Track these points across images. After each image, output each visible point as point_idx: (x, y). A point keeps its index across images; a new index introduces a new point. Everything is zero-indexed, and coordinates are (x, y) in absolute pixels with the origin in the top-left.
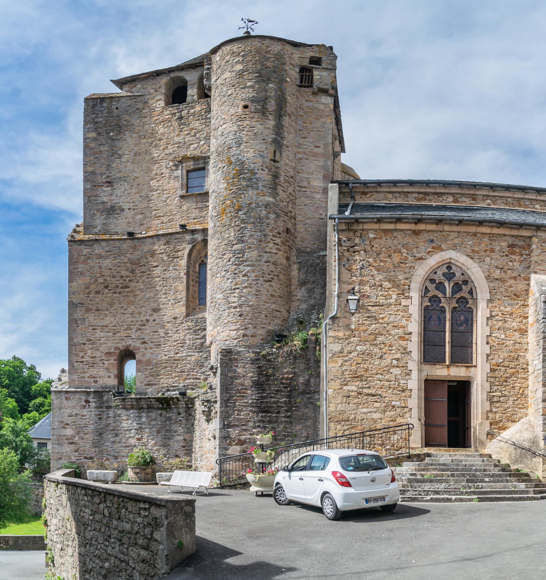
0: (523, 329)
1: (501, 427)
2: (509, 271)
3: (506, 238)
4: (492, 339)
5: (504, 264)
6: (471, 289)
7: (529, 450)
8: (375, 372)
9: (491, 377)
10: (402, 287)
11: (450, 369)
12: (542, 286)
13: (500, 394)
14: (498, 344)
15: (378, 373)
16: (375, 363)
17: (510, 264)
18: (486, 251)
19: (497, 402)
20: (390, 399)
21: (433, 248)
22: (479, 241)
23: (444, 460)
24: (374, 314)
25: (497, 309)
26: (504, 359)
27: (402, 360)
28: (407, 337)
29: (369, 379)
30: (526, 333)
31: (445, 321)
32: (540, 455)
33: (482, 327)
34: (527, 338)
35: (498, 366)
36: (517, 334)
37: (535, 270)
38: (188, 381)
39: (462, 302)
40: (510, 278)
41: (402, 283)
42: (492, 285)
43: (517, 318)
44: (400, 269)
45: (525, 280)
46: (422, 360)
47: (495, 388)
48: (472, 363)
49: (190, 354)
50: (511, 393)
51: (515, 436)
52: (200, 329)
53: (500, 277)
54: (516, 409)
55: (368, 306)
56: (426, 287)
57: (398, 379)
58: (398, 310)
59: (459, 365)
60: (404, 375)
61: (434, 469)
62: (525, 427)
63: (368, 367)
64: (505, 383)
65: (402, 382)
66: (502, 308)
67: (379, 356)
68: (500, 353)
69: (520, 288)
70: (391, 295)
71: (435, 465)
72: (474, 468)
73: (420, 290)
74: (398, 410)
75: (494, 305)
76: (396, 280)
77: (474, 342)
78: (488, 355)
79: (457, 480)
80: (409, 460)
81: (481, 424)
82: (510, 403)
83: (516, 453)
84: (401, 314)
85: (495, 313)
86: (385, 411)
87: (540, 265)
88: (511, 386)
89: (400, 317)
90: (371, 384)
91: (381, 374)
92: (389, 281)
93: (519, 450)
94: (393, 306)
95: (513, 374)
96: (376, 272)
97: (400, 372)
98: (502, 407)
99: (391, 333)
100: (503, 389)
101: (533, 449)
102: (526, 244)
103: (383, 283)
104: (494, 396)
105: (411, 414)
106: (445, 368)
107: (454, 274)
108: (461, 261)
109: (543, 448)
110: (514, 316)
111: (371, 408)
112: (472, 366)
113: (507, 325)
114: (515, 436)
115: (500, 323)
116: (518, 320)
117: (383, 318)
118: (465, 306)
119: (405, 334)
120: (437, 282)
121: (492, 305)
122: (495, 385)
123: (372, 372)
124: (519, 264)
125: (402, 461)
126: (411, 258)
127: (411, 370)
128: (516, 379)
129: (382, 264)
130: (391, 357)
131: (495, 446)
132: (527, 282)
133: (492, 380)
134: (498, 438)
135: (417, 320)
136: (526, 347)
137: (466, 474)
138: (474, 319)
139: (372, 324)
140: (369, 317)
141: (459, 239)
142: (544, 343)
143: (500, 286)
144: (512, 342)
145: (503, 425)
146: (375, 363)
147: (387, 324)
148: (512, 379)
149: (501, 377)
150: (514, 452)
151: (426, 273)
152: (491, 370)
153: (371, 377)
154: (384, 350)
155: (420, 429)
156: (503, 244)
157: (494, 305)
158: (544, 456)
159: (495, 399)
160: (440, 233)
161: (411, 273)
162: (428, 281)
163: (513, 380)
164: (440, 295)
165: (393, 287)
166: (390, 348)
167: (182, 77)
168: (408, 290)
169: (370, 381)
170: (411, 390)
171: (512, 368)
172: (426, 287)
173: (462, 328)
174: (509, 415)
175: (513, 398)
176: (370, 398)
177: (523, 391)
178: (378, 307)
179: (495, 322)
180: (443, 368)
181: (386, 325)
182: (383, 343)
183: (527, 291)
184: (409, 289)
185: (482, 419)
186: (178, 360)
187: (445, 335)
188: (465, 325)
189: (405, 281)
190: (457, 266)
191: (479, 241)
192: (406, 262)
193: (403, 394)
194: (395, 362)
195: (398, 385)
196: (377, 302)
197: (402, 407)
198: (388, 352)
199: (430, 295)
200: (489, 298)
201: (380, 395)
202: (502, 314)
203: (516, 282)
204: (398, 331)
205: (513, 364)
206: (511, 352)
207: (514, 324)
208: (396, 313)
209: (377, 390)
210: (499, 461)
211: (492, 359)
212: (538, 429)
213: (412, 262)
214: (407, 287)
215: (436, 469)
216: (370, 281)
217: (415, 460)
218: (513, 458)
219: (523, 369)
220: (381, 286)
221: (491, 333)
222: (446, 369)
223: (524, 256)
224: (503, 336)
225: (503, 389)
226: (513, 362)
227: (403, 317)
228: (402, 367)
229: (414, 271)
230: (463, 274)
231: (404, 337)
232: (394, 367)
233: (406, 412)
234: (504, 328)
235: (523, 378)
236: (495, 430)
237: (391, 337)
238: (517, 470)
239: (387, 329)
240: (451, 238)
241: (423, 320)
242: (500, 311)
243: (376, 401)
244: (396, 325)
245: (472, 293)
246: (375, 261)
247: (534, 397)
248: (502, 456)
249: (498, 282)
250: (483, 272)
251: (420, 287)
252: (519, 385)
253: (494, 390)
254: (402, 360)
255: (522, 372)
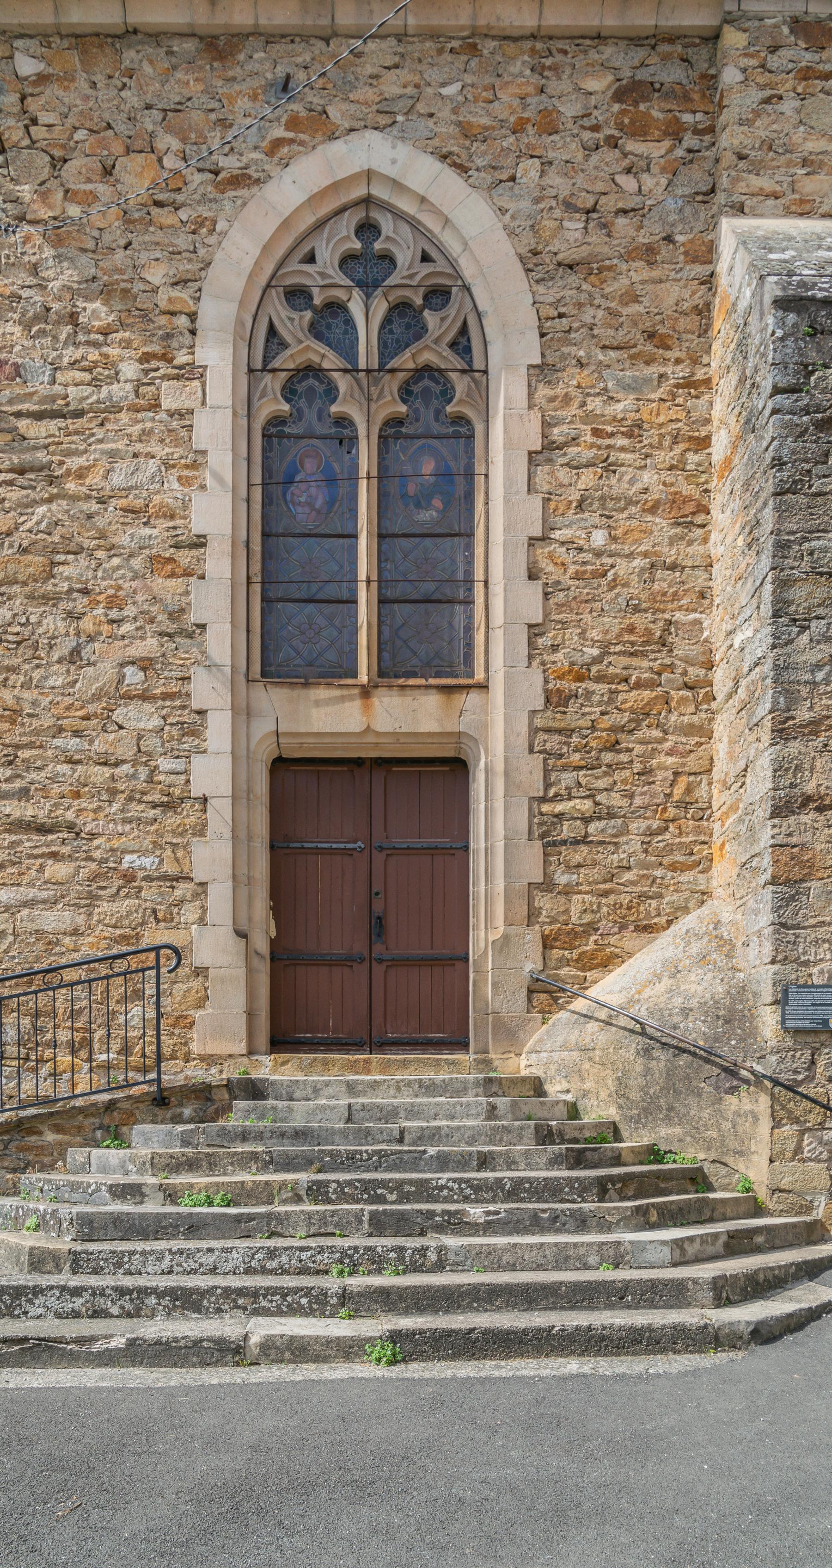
0: (687, 500)
1: (593, 956)
2: (621, 221)
3: (608, 51)
4: (550, 556)
5: (600, 187)
6: (464, 330)
7: (708, 1057)
8: (47, 721)
9: (548, 730)
10: (163, 320)
11: (375, 700)
12: (771, 250)
13: (586, 806)
14: (578, 576)
15: (61, 730)
16: (51, 682)
17: (628, 183)
18: (518, 129)
19: (576, 842)
20: (115, 843)
21: (293, 123)
22: (488, 80)
23: (311, 1114)
24: (42, 456)
25: (573, 409)
26: (605, 647)
27: (165, 664)
28: (185, 557)
29: (24, 754)
30: (700, 519)
31: (354, 479)
32: (759, 1078)
33: (507, 500)
34: (705, 540)
35: (580, 678)
36: (660, 523)
37: (737, 198)
39: (426, 393)
40: (629, 256)
41: (163, 305)
42: (548, 294)
43: (660, 447)
44: (154, 235)
45: (695, 260)
46: (257, 667)
47: (567, 778)
48: (471, 675)
50: (638, 801)
51: (647, 992)
53: (584, 251)
54: (659, 873)
55: (18, 415)
56: (272, 331)
57: (149, 754)
58: (146, 434)
59: (412, 682)
60: (175, 732)
61: (245, 1161)
62: (695, 948)
63: (18, 699)
64: (608, 757)
65: (165, 764)
66: (595, 404)
67: (66, 652)
68: (587, 618)
69: (671, 301)
70: (114, 365)
71: (260, 1137)
72: (432, 1151)
73: (237, 336)
74: (150, 893)
75: (560, 390)
76: (138, 286)
77: (479, 574)
78: (535, 631)
79: (323, 1217)
80: (160, 1113)
81: (504, 944)
82: (633, 844)
83: (647, 1071)
84: (161, 451)
85: (565, 428)
86: (93, 897)
87: (757, 169)
88: (637, 767)
89: (152, 466)
90: (33, 775)
91: (77, 733)
92: (106, 293)
93: (662, 1056)
94: (124, 417)
95: (643, 714)
96: (48, 252)
97: (156, 722)
98: (595, 863)
99: (115, 540)
100: (602, 783)
101: (725, 1051)
102: (694, 75)
103: (80, 304)
104: (560, 816)
105: (204, 909)
106: (351, 698)
107: (388, 259)
108: (416, 182)
109: (773, 1043)
110: (650, 436)
111: (31, 885)
112: (469, 687)
113: (617, 485)
114: (647, 992)
115: (587, 478)
116: (663, 457)
117: (81, 474)
118: (438, 413)
119: (177, 546)
120: (317, 301)
121: (549, 392)
122: (564, 768)
123: (36, 723)
124: (664, 181)
125: (130, 1119)
126: (198, 178)
127: (201, 713)
128: (656, 733)
129: (74, 211)
130: (118, 651)
131: (560, 1039)
132: (700, 270)
133: (553, 742)
134: (579, 1004)
135: (228, 477)
136: (699, 580)
137: (383, 1184)
138: (480, 468)
139: (35, 503)
140: (21, 472)
141: (404, 75)
142: (780, 519)
143: (583, 297)
144: (637, 562)
145: (600, 947)
146: (51, 682)
147: (102, 501)
148: (639, 734)
149: (593, 728)
150: (639, 1068)
151: (266, 249)
152: (548, 700)
153: (31, 745)
154: (87, 624)
155: (242, 972)
156: (593, 84)
157: (560, 390)
158: (776, 1082)
159: (566, 830)
160: (321, 44)
161: (202, 252)
162: (276, 301)
163: (642, 742)
164: (331, 360)
165: (123, 325)
166: (114, 614)
168: (187, 339)
169: (28, 765)
170: (205, 800)
171: (638, 685)
172: (272, 331)
173: (427, 516)
174: (625, 899)
175: (643, 824)
176: (29, 842)
177: (689, 790)
178: (61, 423)
179: (563, 475)
180: (342, 699)
181: (94, 507)
182: (85, 592)
183: (704, 311)
184: (193, 332)
185: (508, 923)
187: (353, 551)
188: (437, 503)
189: (176, 293)
190: (399, 215)
191: (488, 80)
192: (180, 198)
193: (172, 820)
194: (133, 676)
195: (150, 780)
196: (53, 399)
197: (165, 878)
198: (105, 628)
199: (286, 360)
200: (538, 361)
201: (71, 827)
202: (596, 433)
203: (655, 274)
204: (147, 531)
205: (645, 664)
206: (637, 609)
207: (648, 478)
208: (138, 447)
209: (56, 805)
210: (573, 1111)
211: (555, 648)
212: (752, 952)
213: (204, 199)
214: (182, 321)
215: (254, 1156)
216: (25, 293)
217: (187, 1112)
218: (634, 1095)
219: (687, 686)
220: (73, 318)
221: (549, 527)
222: (358, 703)
223: (690, 140)
224: (599, 538)
225: (602, 783)
226: (643, 654)
227: (168, 466)
228: (166, 696)
229: (212, 240)
230: (426, 258)
231: (171, 560)
232: (129, 697)
233: (181, 902)
234: (603, 498)
235: (689, 730)
236: (564, 971)
237: (116, 561)
238: (653, 1154)
239: (100, 522)
240: (369, 70)
241: (257, 479)
242: (589, 418)
243: (54, 855)
244: (139, 503)
245: (468, 350)
246: (44, 196)
247: (734, 808)
248: (588, 1085)
249: (573, 279)
250: (512, 233)
251: (240, 322)
252: (670, 760)
253: (561, 788)
254: (165, 664)
255: (683, 700)
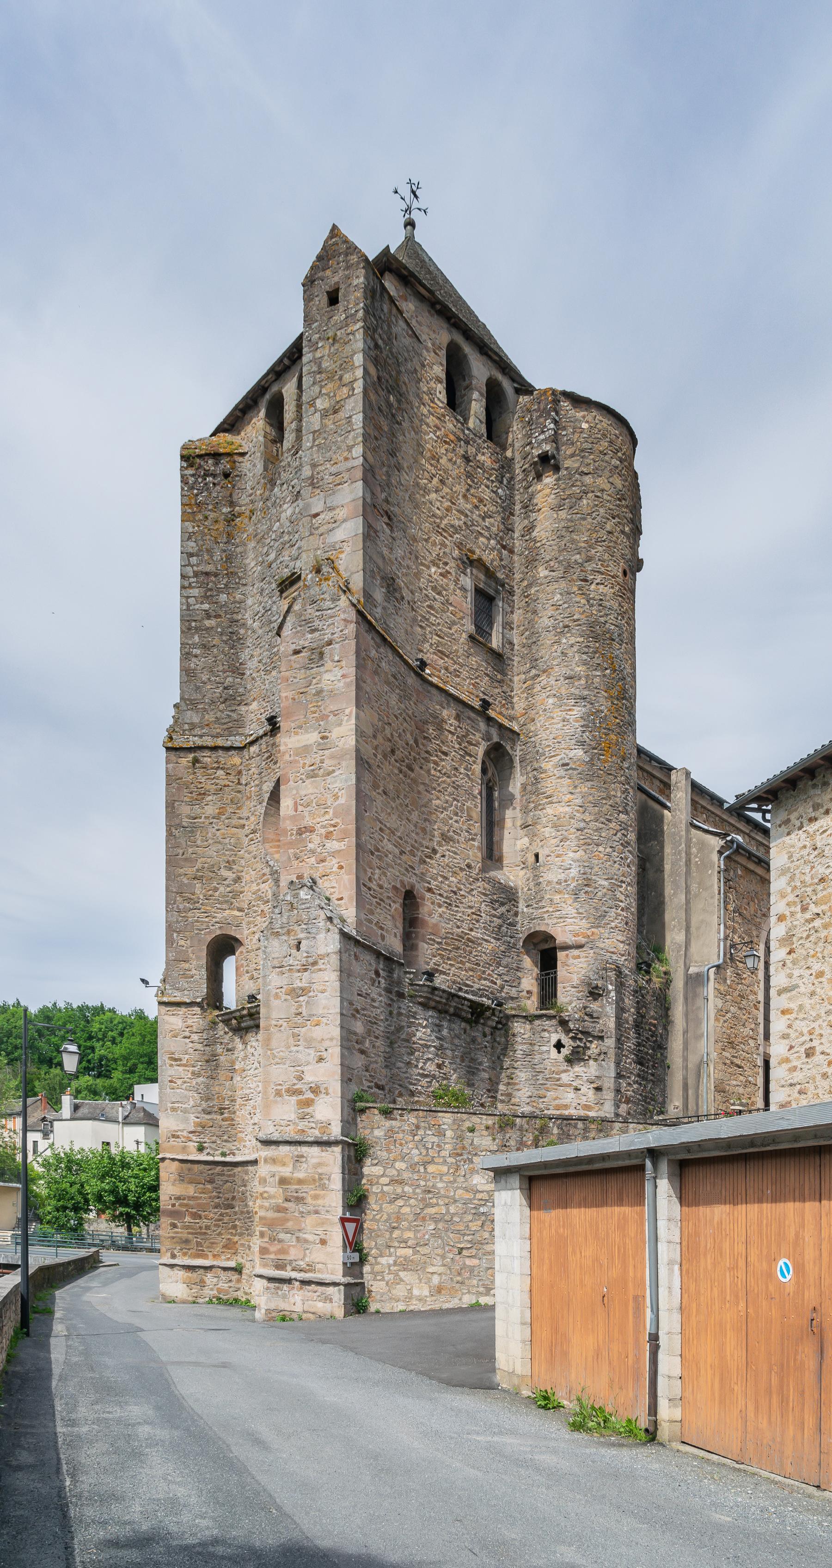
38: (484, 982)
49: (486, 938)
52: (497, 901)
55: (795, 1360)
167: (465, 356)
186: (473, 942)
